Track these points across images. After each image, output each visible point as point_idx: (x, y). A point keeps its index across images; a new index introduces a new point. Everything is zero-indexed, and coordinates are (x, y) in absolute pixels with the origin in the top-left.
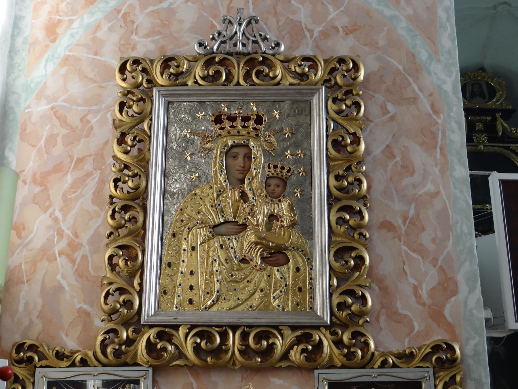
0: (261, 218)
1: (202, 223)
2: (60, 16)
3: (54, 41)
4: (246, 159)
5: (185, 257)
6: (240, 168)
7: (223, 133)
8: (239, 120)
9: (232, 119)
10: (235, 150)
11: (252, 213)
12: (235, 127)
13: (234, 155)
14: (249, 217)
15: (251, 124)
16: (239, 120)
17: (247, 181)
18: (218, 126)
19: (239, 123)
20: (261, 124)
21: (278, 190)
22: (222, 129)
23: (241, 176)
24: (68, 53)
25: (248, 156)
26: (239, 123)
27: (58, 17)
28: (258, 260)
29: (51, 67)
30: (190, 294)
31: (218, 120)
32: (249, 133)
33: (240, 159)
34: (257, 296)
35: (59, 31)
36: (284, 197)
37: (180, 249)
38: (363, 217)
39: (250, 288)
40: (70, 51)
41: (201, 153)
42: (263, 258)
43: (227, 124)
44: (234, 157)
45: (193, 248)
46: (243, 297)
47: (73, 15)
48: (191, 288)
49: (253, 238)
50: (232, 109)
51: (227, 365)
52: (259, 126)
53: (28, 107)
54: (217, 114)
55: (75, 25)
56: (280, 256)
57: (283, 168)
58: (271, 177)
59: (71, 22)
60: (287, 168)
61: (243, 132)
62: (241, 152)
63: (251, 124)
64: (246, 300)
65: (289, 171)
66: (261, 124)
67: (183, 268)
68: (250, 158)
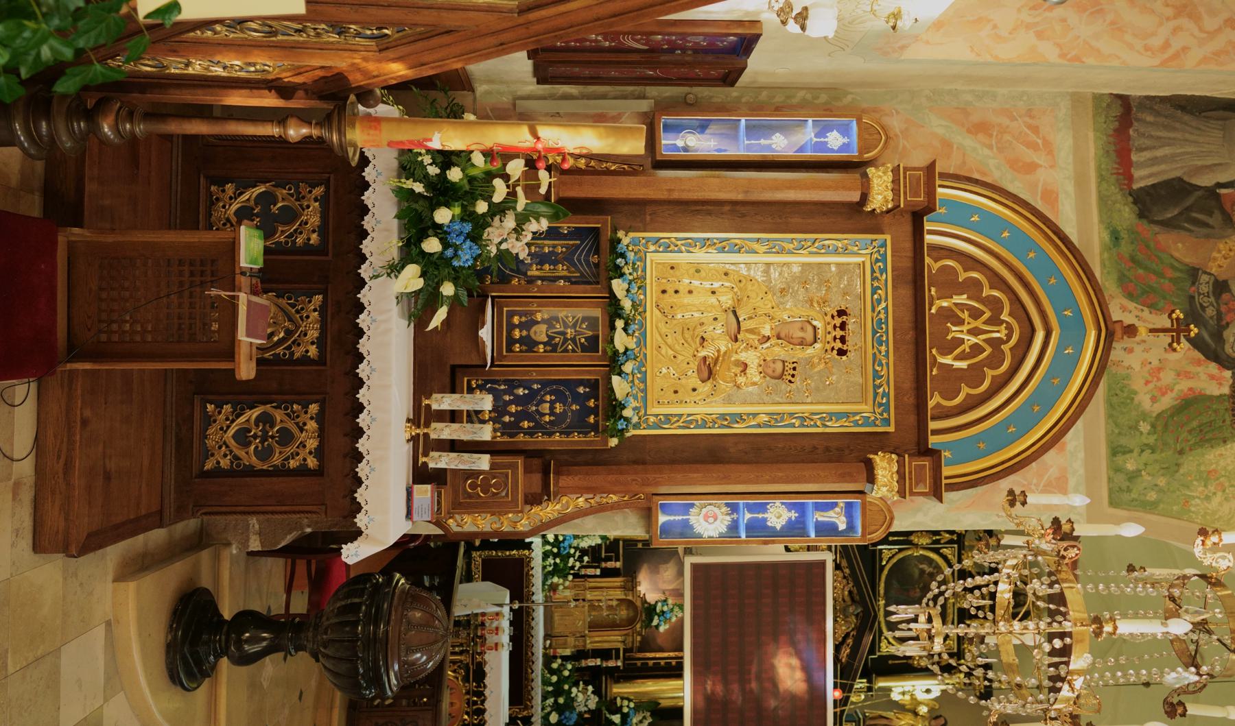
0: (743, 356)
1: (738, 300)
2: (997, 135)
3: (969, 131)
4: (800, 340)
5: (707, 285)
6: (791, 333)
7: (828, 318)
8: (842, 333)
9: (843, 326)
10: (810, 329)
11: (750, 346)
12: (835, 329)
13: (805, 328)
14: (745, 344)
15: (838, 345)
16: (842, 333)
17: (780, 341)
18: (836, 314)
19: (839, 333)
20: (838, 354)
21: (770, 371)
22: (833, 317)
23: (782, 335)
24: (955, 147)
25: (803, 343)
26: (839, 333)
27: (995, 134)
28: (703, 353)
29: (940, 131)
30: (671, 291)
31: (841, 313)
32: (828, 342)
33: (801, 334)
34: (671, 353)
35: (981, 136)
36: (765, 377)
37: (713, 280)
38: (451, 671)
39: (677, 347)
40: (957, 148)
41: (718, 357)
42: (705, 358)
43: (838, 321)
44: (802, 328)
45: (713, 293)
46: (669, 340)
47: (998, 148)
48: (676, 292)
49: (723, 349)
50: (854, 326)
51: (625, 316)
52: (835, 352)
53: (898, 113)
54: (848, 312)
55: (986, 151)
56: (706, 374)
57: (793, 376)
58: (784, 365)
59: (990, 147)
60: (793, 380)
61: (830, 338)
62: (809, 336)
63: (838, 345)
64: (666, 343)
65: (790, 381)
66: (838, 354)
67: (696, 283)
68: (801, 344)
